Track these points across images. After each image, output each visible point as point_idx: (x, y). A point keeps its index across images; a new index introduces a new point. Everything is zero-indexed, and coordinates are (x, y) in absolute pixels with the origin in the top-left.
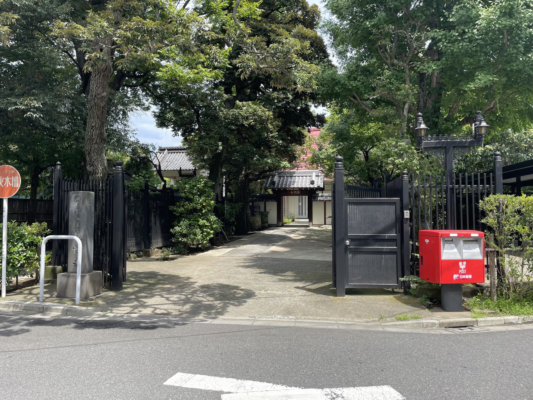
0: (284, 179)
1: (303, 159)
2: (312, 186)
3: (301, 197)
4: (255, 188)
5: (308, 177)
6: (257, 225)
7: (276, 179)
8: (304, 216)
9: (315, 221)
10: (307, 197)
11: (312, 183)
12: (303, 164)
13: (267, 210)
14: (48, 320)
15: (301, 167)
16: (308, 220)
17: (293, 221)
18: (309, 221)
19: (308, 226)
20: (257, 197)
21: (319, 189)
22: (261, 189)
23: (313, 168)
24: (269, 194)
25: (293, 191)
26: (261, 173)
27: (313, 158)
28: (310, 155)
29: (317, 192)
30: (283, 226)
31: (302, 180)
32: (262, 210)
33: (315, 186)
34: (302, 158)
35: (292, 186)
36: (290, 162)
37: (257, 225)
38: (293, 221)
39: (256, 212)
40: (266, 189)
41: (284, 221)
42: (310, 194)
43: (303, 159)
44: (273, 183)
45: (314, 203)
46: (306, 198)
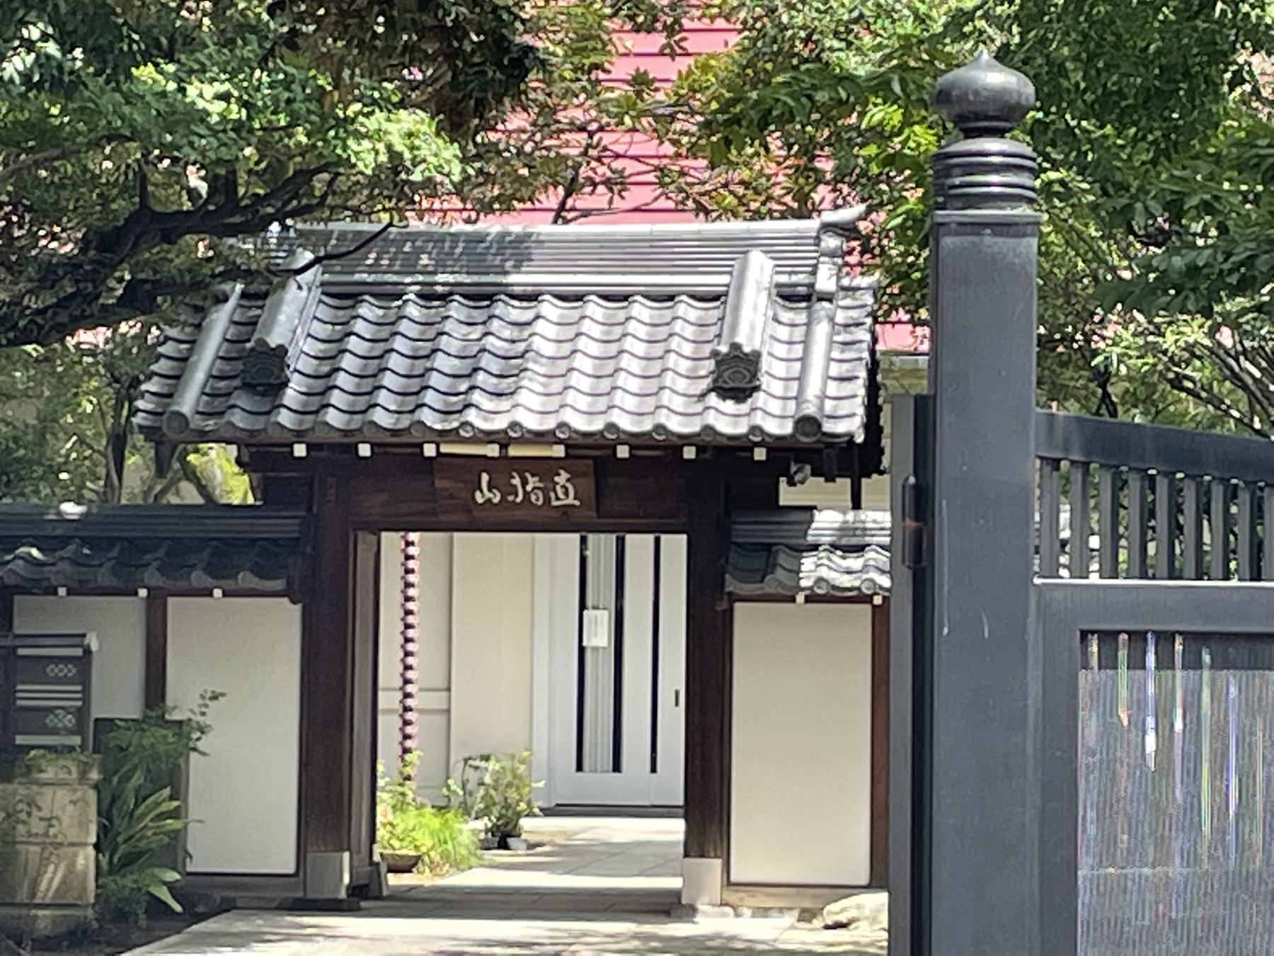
0: (390, 326)
1: (641, 82)
2: (727, 419)
3: (601, 544)
4: (48, 422)
5: (688, 310)
6: (50, 881)
7: (296, 320)
8: (635, 780)
9: (756, 846)
10: (676, 546)
11: (736, 375)
12: (635, 145)
13: (183, 697)
14: (1027, 174)
15: (617, 184)
16: (676, 829)
17: (502, 837)
18: (696, 846)
19: (669, 906)
20: (56, 537)
21: (812, 451)
22: (119, 444)
23: (753, 201)
24: (212, 506)
25: (503, 467)
26: (107, 244)
27: (750, 71)
28: (717, 45)
29: (788, 495)
30: (365, 896)
31: (615, 339)
32: (117, 695)
33: (771, 414)
34: (622, 69)
35: (488, 415)
36: (458, 113)
37: (50, 881)
38: (502, 837)
39: (38, 719)
40: (171, 443)
41: (388, 843)
42: (711, 503)
43: (641, 82)
44: (259, 370)
45: (749, 621)
46: (659, 565)
